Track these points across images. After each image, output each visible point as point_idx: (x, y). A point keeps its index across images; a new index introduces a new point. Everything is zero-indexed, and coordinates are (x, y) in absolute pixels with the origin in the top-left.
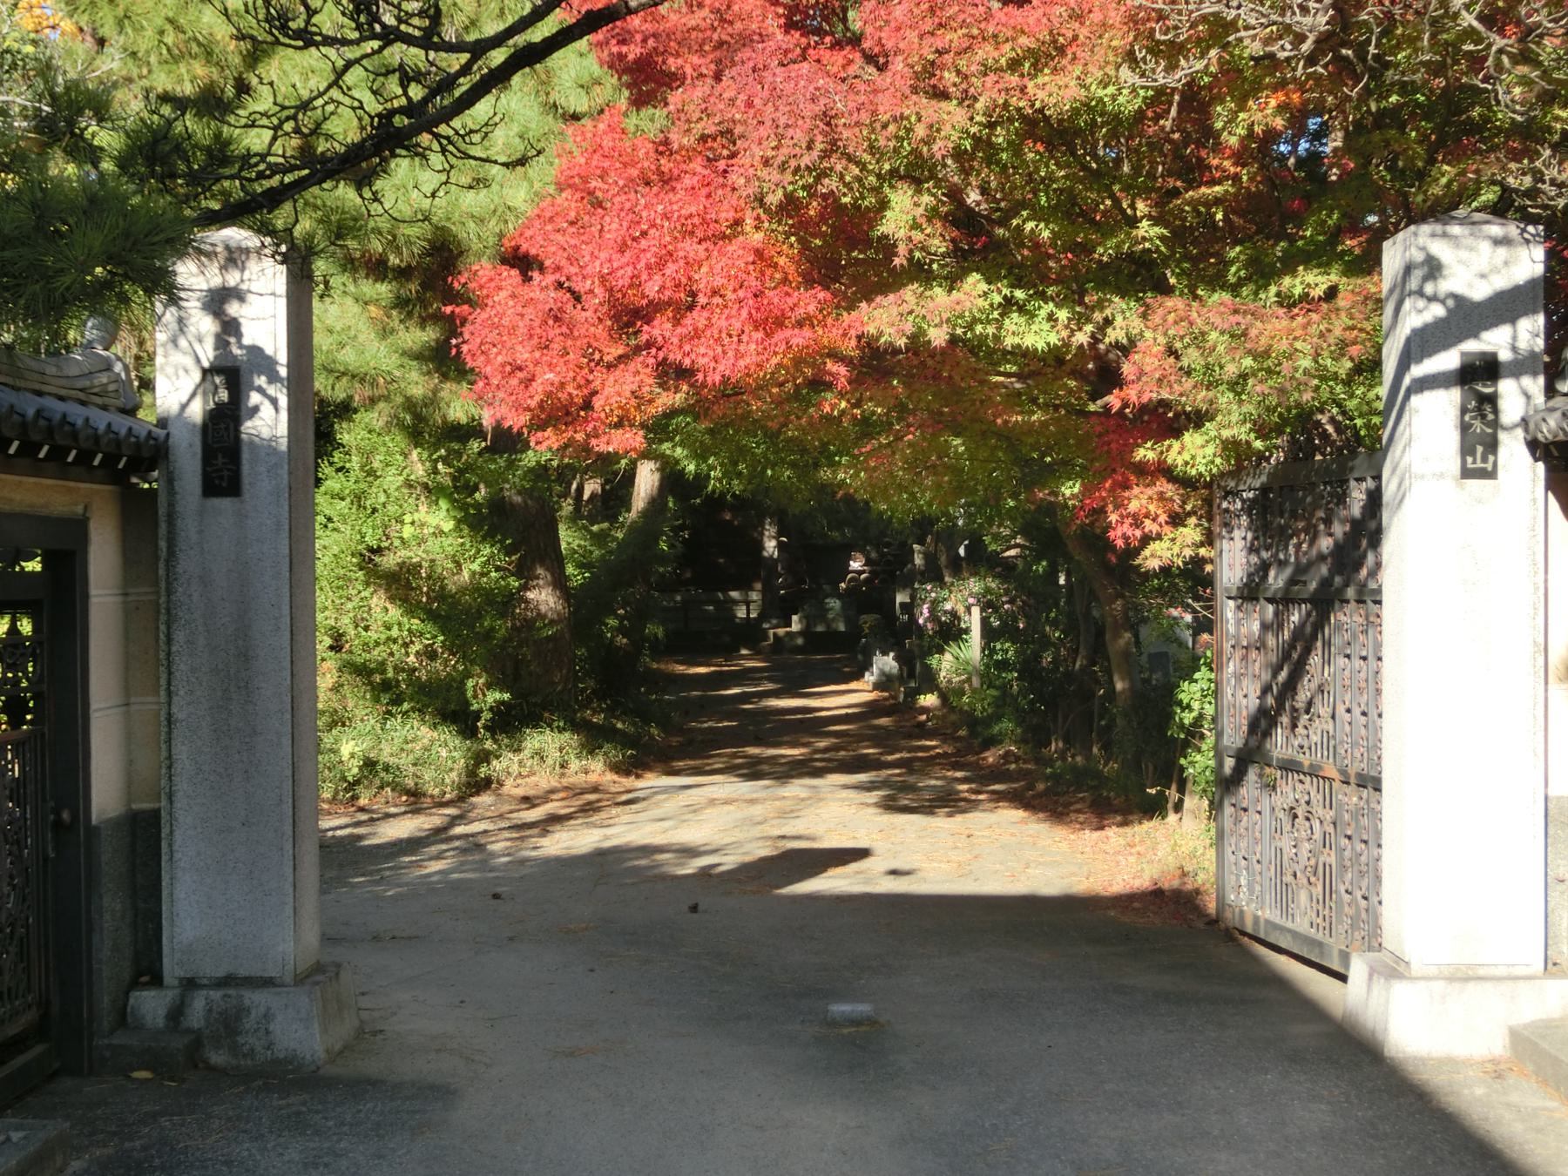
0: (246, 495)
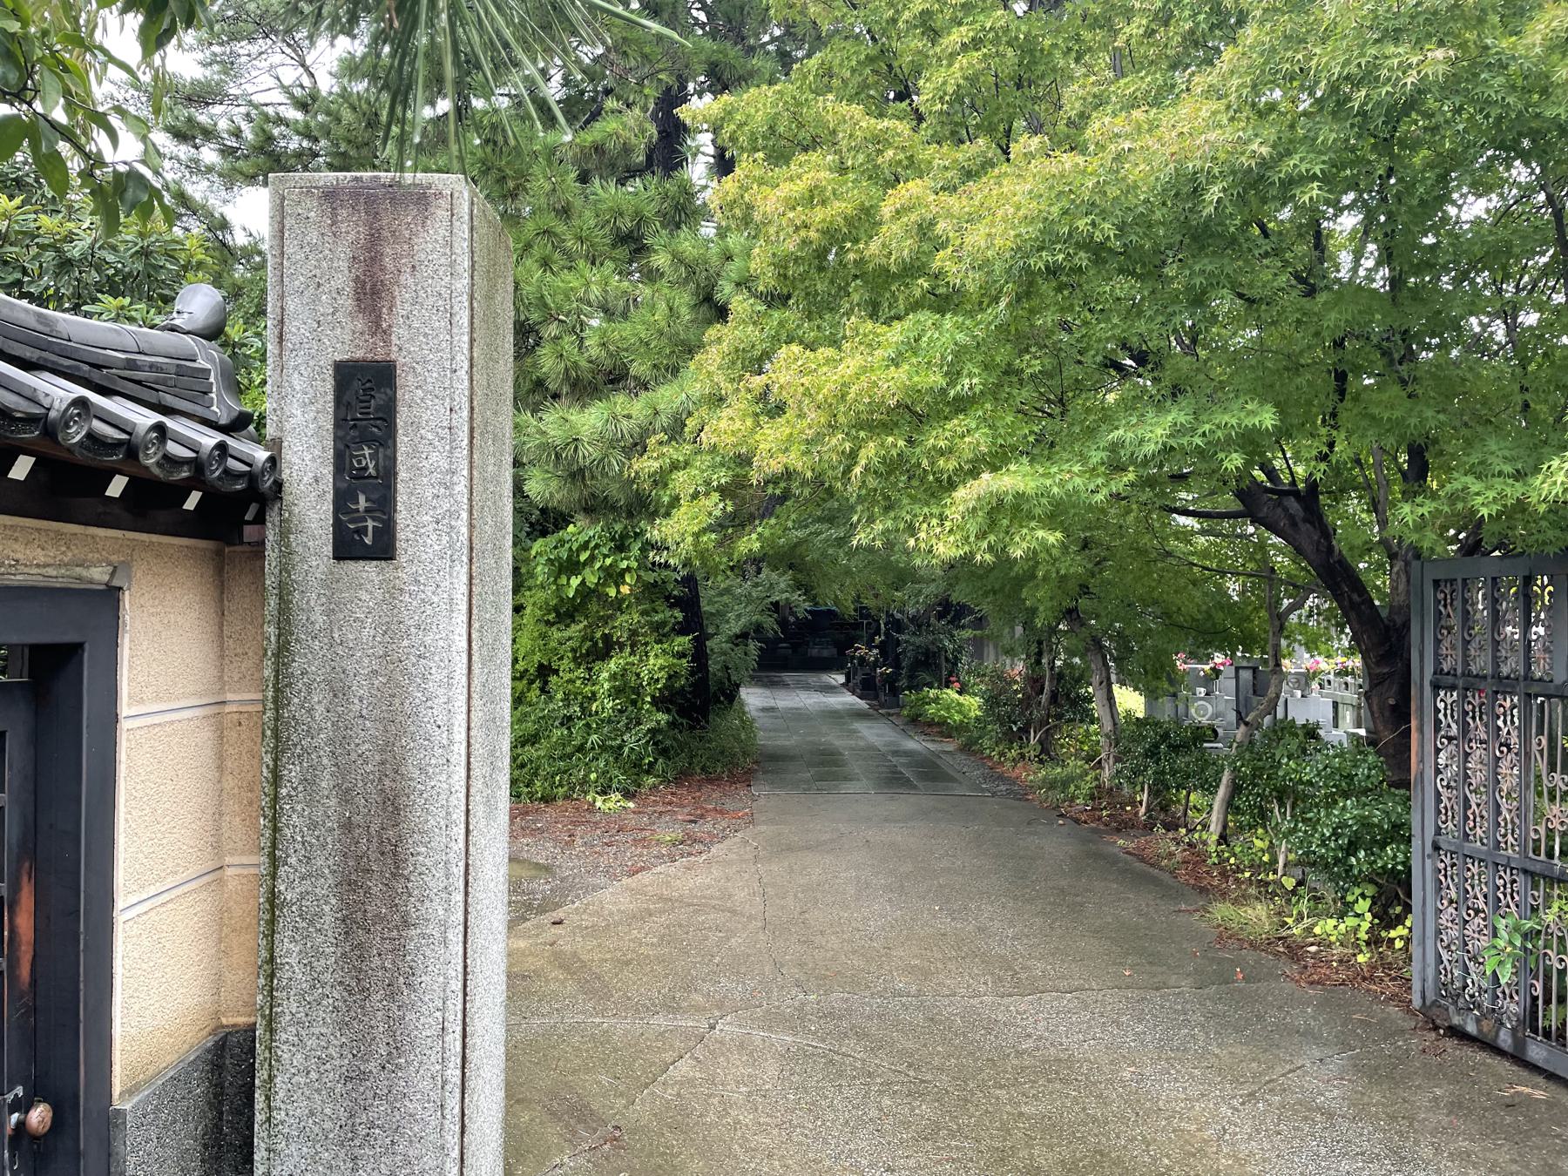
0: (402, 558)
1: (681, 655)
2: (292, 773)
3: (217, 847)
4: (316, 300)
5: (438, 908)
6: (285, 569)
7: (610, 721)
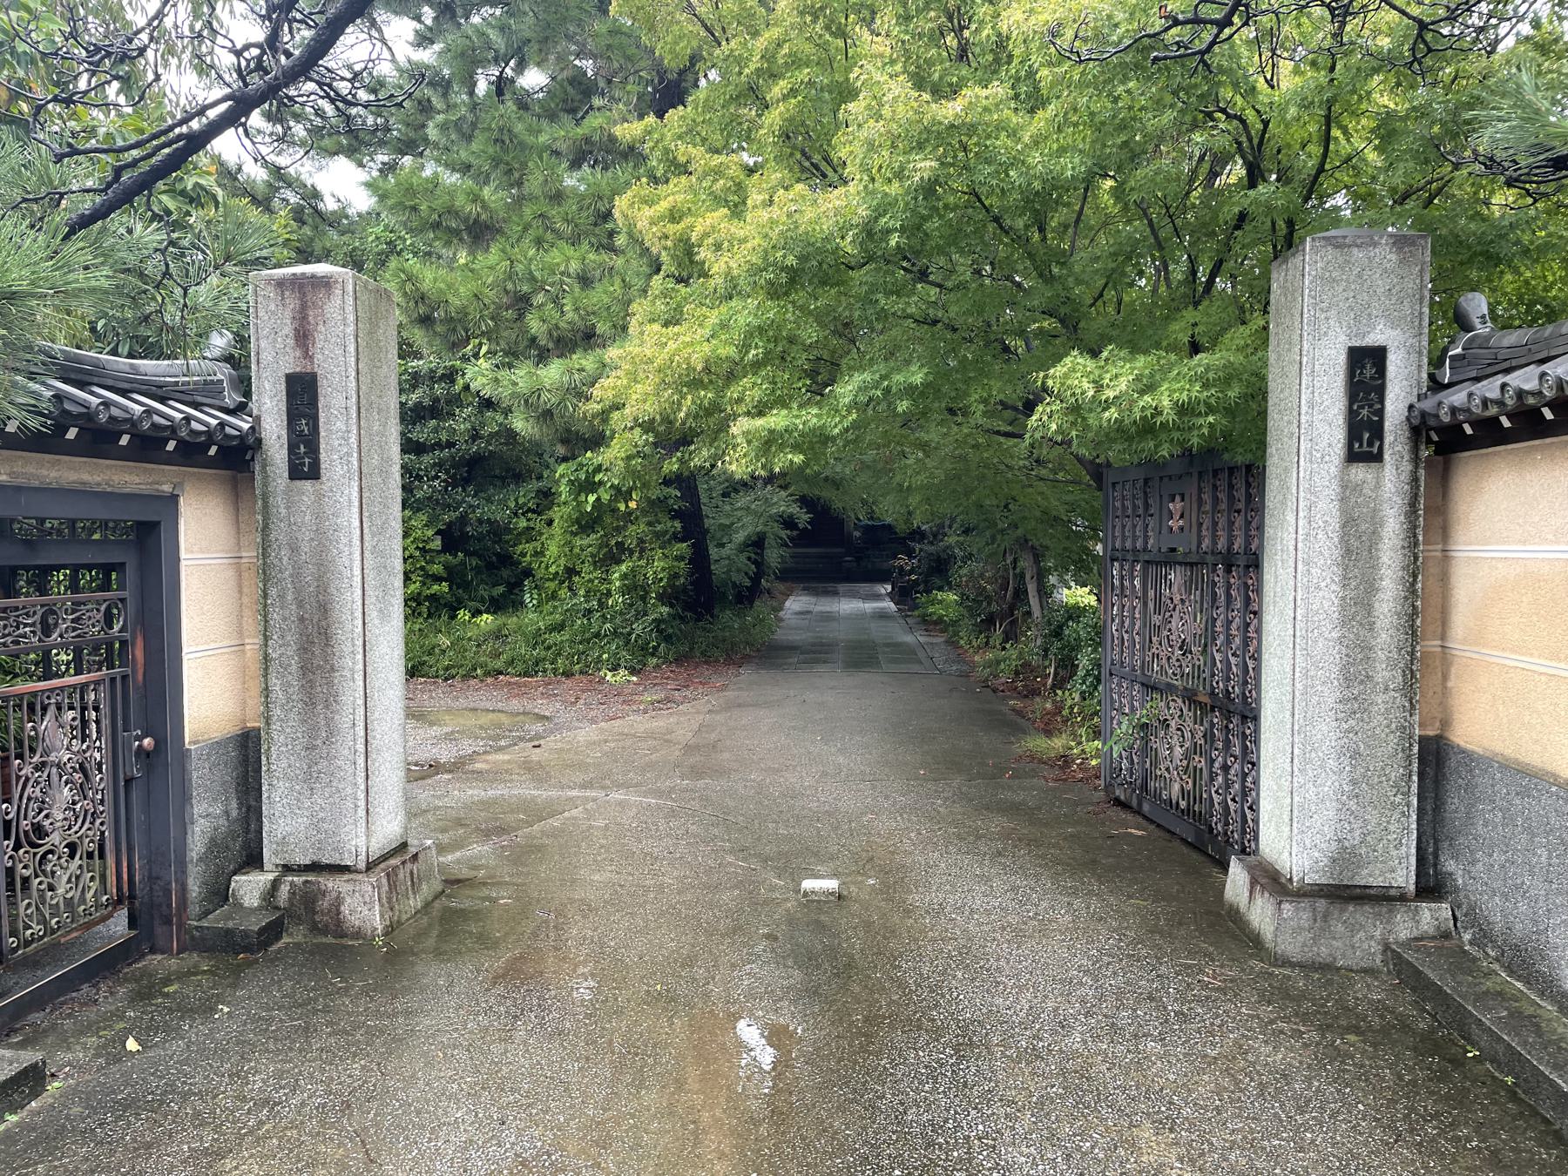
0: (324, 479)
1: (680, 558)
2: (273, 592)
3: (240, 633)
4: (275, 341)
5: (349, 661)
6: (265, 485)
7: (621, 614)
